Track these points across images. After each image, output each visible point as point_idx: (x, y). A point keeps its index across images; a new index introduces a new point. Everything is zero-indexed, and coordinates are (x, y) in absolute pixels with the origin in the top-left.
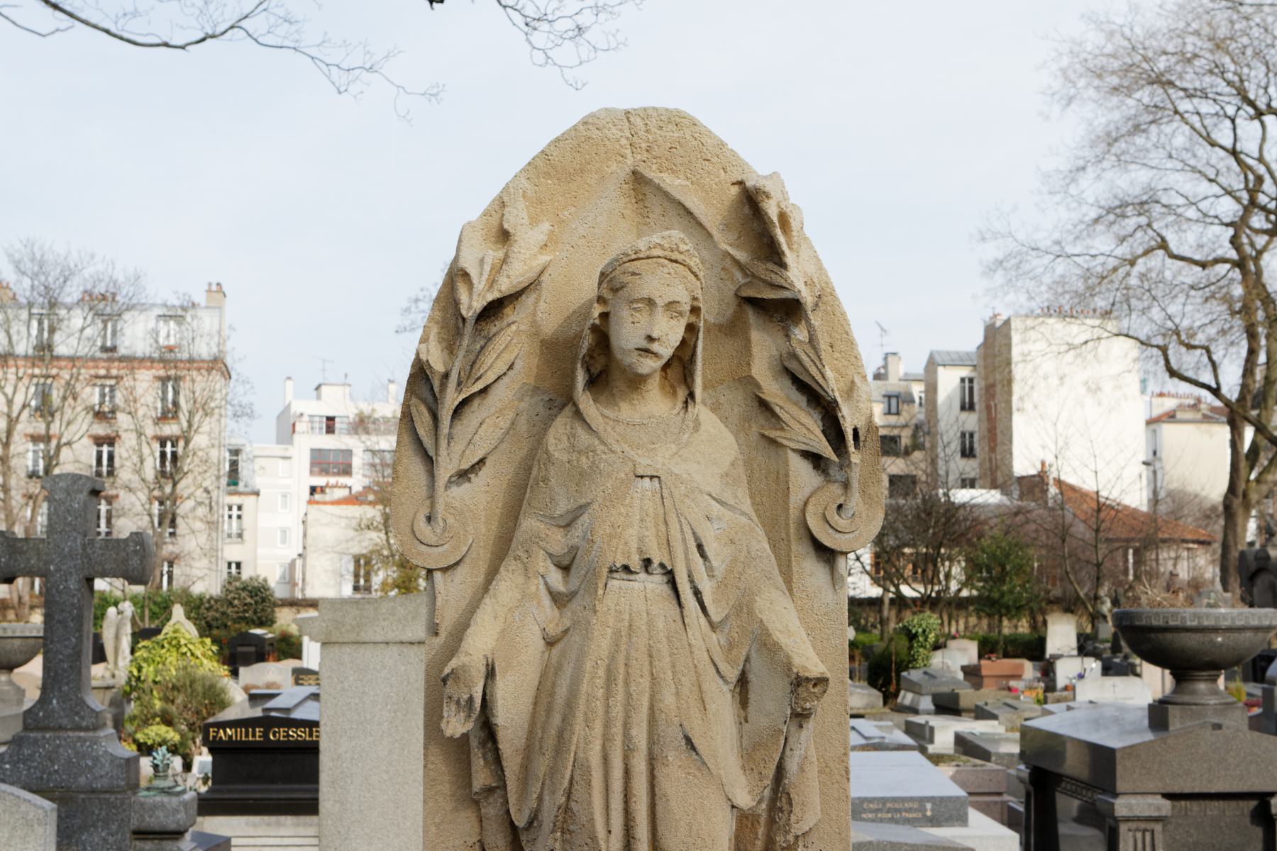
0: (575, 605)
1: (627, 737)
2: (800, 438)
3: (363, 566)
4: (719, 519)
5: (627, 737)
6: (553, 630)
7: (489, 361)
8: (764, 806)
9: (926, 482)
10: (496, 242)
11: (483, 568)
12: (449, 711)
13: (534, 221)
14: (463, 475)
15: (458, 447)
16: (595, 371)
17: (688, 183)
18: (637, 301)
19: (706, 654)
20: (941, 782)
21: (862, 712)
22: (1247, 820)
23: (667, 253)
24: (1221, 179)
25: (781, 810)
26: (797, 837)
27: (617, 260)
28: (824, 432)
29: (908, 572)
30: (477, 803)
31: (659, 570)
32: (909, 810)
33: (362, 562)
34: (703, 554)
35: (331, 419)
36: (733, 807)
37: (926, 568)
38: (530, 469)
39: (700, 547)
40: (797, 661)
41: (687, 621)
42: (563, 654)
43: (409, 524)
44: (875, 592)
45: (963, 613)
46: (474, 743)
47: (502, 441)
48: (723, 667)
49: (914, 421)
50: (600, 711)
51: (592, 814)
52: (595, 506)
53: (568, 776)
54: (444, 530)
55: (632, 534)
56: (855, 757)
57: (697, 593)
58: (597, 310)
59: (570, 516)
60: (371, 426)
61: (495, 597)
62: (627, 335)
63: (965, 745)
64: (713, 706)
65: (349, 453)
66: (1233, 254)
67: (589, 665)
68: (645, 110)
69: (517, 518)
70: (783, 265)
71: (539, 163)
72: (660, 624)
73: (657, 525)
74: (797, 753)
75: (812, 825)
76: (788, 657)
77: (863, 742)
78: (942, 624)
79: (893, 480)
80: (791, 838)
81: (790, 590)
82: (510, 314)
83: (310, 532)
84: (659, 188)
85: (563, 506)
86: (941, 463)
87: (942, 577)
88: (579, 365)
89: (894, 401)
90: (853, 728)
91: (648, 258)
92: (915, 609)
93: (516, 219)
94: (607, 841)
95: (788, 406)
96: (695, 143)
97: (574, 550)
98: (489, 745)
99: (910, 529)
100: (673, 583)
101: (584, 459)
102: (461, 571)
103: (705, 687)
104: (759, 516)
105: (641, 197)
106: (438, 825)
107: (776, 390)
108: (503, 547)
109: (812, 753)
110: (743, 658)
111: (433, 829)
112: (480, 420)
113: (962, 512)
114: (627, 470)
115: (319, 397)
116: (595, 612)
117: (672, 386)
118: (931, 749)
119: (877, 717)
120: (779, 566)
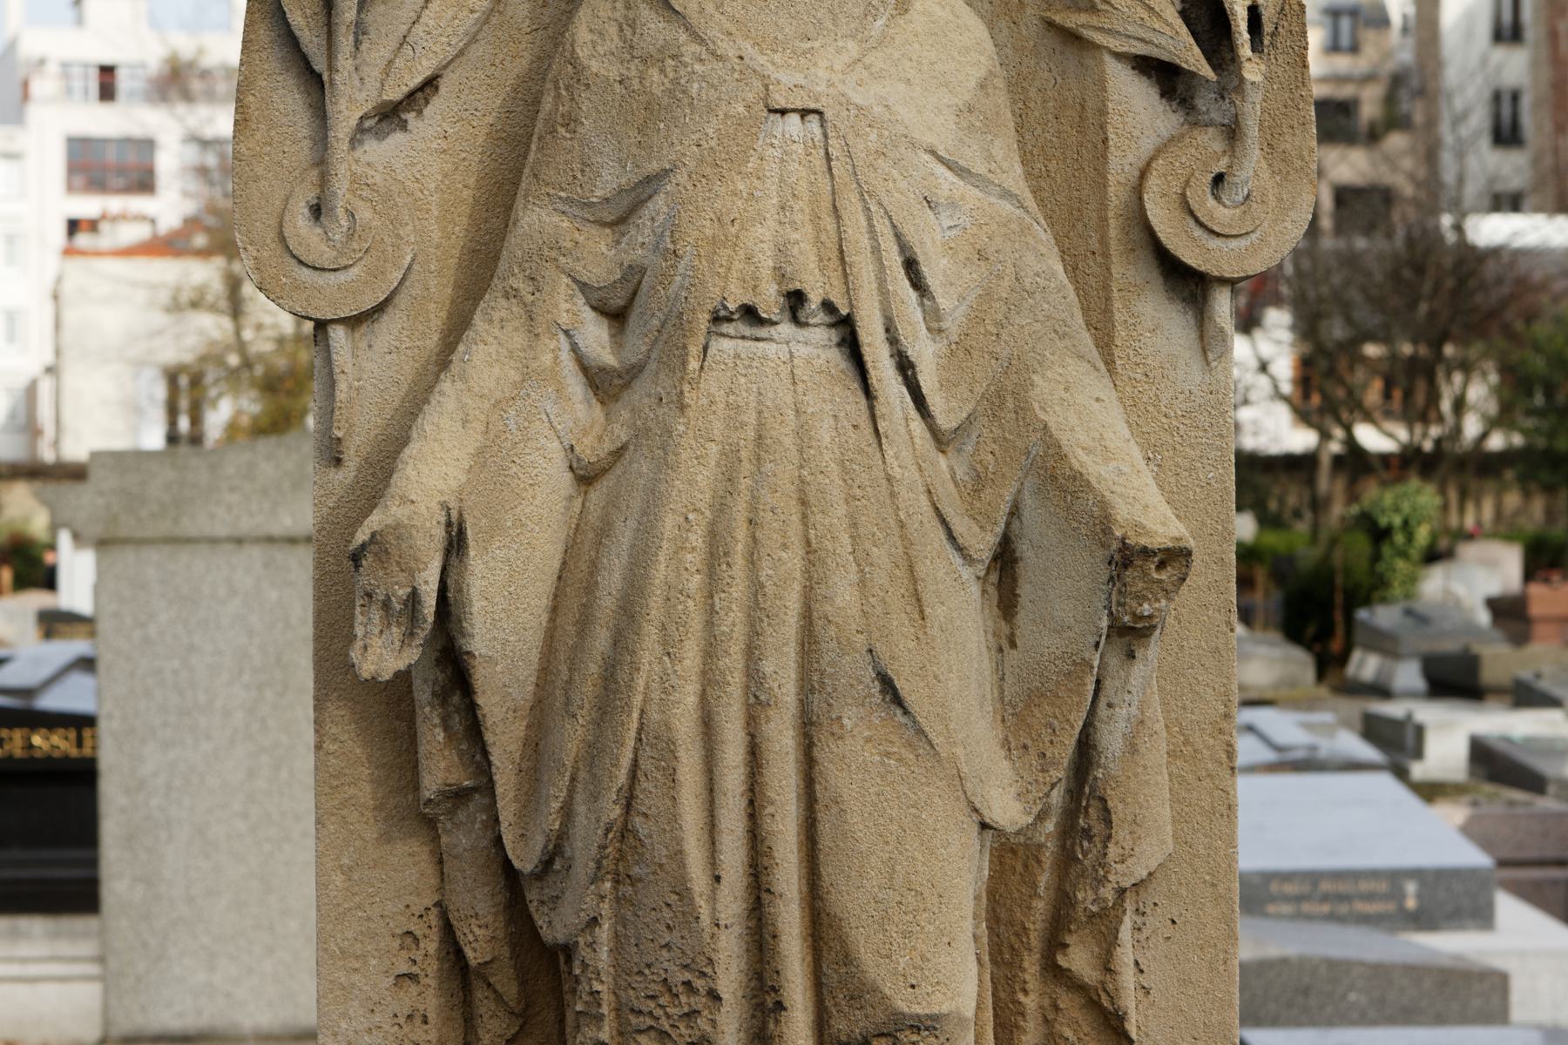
0: (639, 394)
1: (753, 676)
2: (1131, 29)
3: (185, 389)
4: (953, 205)
5: (753, 676)
6: (592, 450)
8: (1050, 826)
9: (1415, 202)
11: (436, 317)
12: (367, 623)
14: (390, 115)
15: (377, 52)
19: (924, 499)
20: (1440, 839)
21: (1269, 695)
25: (1087, 834)
26: (1121, 892)
28: (1183, 14)
29: (1373, 395)
30: (430, 823)
31: (821, 317)
32: (1370, 897)
33: (184, 381)
35: (107, 71)
36: (984, 826)
37: (1412, 389)
38: (537, 101)
39: (911, 265)
40: (1123, 512)
41: (882, 426)
42: (613, 502)
43: (273, 222)
44: (1300, 440)
45: (1490, 484)
46: (423, 693)
47: (474, 39)
48: (961, 525)
49: (1390, 67)
50: (696, 622)
51: (679, 841)
55: (761, 239)
56: (1248, 789)
57: (905, 367)
59: (626, 202)
60: (196, 85)
61: (464, 378)
63: (1488, 761)
64: (941, 610)
65: (147, 145)
67: (669, 524)
69: (509, 208)
73: (816, 218)
74: (1122, 712)
75: (1153, 865)
76: (1104, 505)
77: (1269, 756)
78: (1445, 508)
79: (1343, 196)
80: (1108, 893)
81: (1110, 363)
83: (70, 316)
85: (609, 179)
86: (1447, 159)
87: (1446, 406)
89: (1345, 24)
90: (1250, 729)
92: (1385, 475)
94: (713, 899)
97: (634, 276)
98: (456, 699)
99: (1378, 303)
100: (851, 345)
101: (654, 74)
102: (389, 328)
103: (922, 569)
104: (1041, 203)
106: (347, 871)
108: (480, 270)
109: (1156, 713)
110: (1005, 508)
111: (338, 879)
113: (1490, 269)
114: (750, 96)
115: (80, 21)
116: (682, 408)
118: (1418, 771)
120: (1086, 311)
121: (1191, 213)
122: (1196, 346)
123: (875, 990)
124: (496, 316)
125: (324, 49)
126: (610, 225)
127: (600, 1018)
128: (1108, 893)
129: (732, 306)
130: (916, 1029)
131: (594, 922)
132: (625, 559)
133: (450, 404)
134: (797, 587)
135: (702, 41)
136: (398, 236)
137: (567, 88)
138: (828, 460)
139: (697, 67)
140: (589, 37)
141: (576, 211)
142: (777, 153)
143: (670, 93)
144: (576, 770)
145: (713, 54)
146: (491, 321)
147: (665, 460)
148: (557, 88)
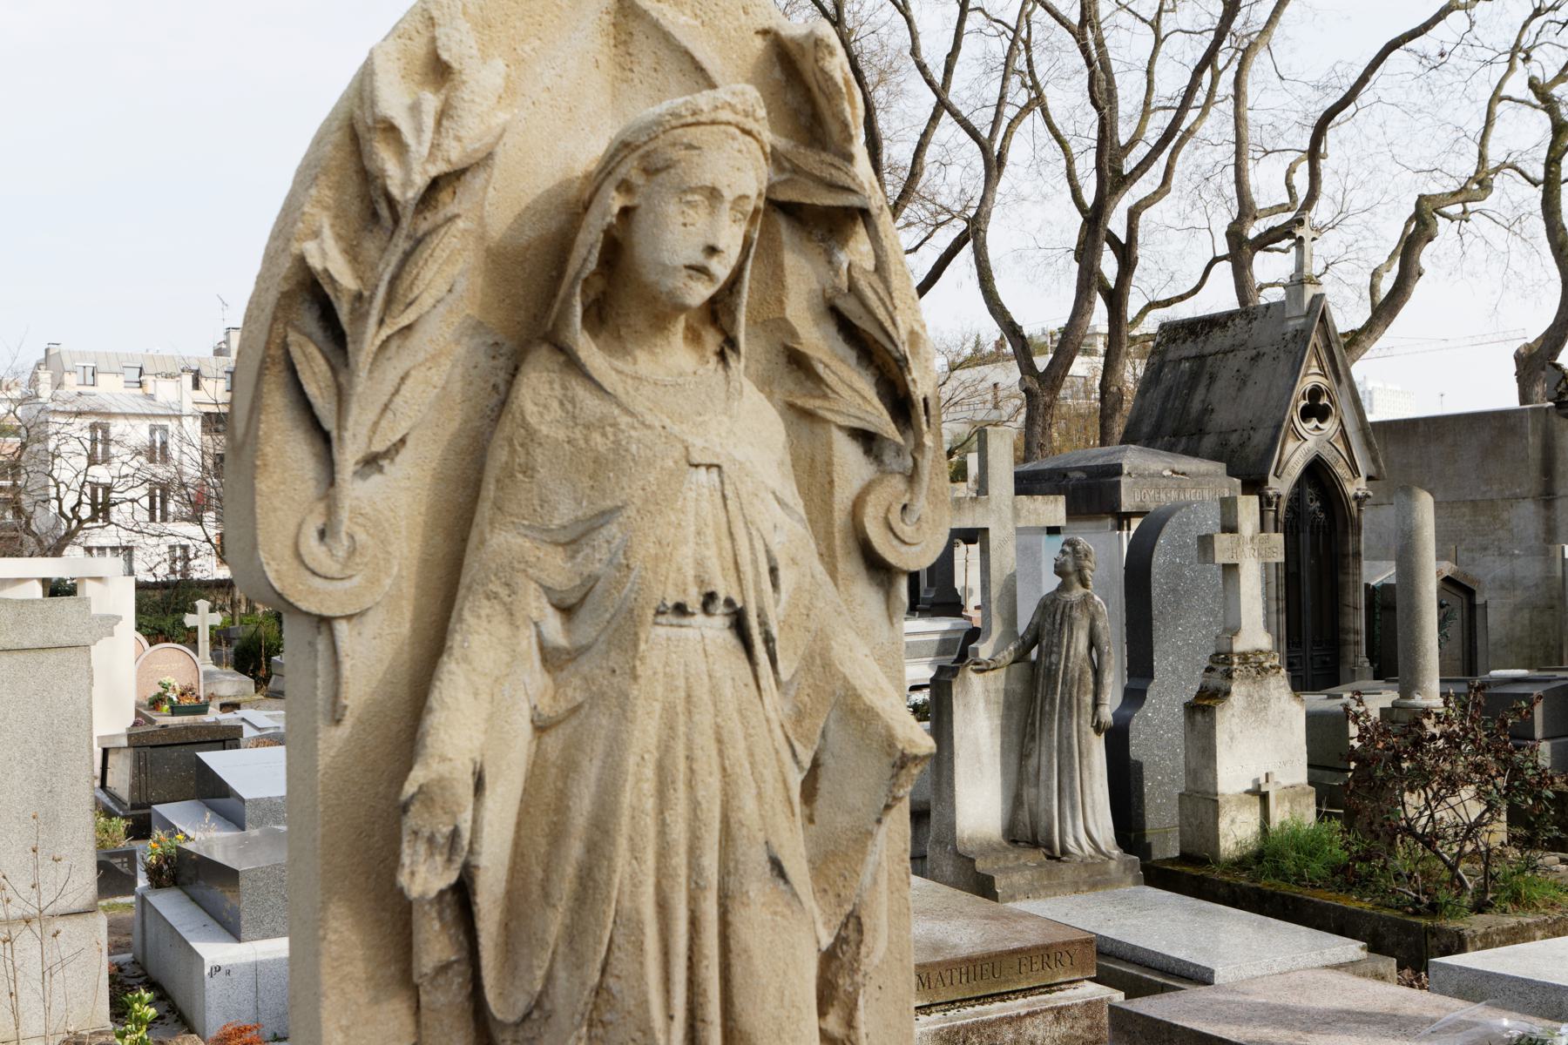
0: (585, 665)
2: (852, 411)
6: (547, 708)
7: (428, 274)
13: (485, 58)
14: (372, 462)
23: (739, 119)
27: (659, 124)
39: (773, 571)
43: (290, 543)
48: (798, 747)
50: (651, 832)
51: (645, 993)
52: (631, 511)
53: (606, 940)
54: (352, 552)
55: (686, 555)
58: (616, 202)
59: (581, 528)
61: (466, 659)
67: (632, 761)
72: (727, 691)
73: (718, 539)
76: (888, 728)
82: (449, 205)
84: (656, 26)
85: (565, 512)
91: (713, 123)
93: (458, 45)
94: (668, 1032)
95: (834, 364)
97: (589, 586)
101: (596, 437)
102: (371, 624)
105: (624, 37)
107: (817, 340)
116: (635, 678)
119: (255, 706)
121: (891, 529)
122: (885, 613)
124: (483, 613)
125: (334, 414)
129: (670, 604)
132: (593, 789)
133: (461, 681)
134: (718, 802)
135: (632, 414)
136: (388, 553)
137: (522, 445)
138: (731, 709)
139: (633, 433)
140: (535, 409)
141: (536, 534)
142: (694, 495)
143: (615, 451)
144: (556, 945)
145: (643, 423)
146: (479, 617)
148: (511, 445)
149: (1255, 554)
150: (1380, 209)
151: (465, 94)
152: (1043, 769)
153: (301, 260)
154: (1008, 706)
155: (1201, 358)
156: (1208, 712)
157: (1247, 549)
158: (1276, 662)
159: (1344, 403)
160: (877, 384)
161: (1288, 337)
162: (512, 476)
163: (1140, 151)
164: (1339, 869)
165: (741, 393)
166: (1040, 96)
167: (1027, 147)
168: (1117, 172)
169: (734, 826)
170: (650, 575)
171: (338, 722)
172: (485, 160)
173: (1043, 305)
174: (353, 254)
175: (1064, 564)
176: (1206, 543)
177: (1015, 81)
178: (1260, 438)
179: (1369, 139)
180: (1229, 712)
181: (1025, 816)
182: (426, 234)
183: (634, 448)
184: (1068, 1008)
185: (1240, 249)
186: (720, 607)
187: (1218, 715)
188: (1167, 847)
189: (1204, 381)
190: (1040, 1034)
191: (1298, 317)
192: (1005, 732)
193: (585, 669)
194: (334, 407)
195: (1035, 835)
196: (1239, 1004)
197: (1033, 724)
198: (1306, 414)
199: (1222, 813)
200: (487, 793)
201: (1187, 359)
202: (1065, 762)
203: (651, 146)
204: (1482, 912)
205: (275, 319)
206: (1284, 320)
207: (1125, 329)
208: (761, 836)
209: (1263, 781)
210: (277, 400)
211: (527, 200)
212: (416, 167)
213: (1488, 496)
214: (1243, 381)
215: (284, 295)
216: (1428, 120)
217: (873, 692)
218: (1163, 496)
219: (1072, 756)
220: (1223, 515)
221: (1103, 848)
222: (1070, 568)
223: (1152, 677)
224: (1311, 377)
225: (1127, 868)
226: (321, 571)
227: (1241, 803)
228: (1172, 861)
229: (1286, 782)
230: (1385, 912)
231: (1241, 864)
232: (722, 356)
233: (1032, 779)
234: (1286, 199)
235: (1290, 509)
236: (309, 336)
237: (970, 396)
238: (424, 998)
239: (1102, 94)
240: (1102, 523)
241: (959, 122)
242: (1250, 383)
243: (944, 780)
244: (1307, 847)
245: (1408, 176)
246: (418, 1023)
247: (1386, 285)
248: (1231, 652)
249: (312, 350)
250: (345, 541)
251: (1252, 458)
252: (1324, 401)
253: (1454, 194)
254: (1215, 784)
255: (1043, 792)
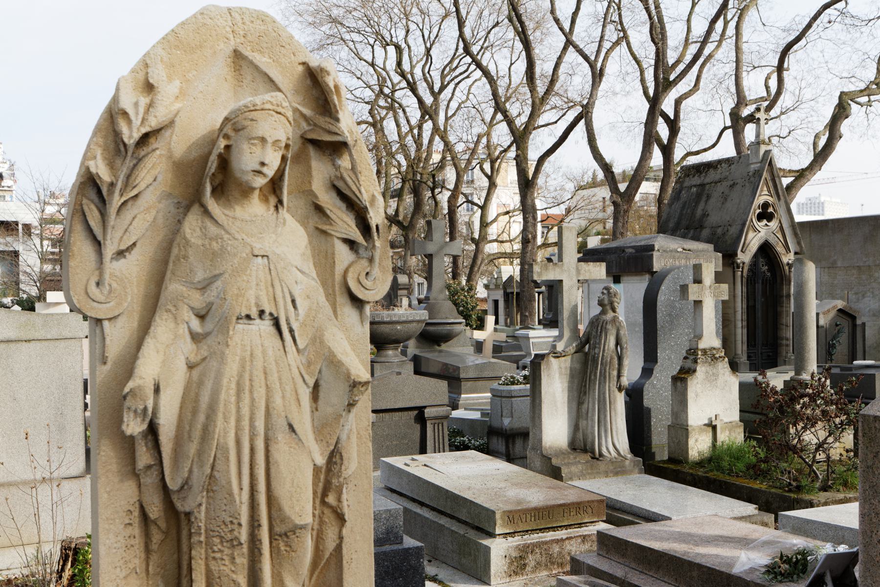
0: (210, 340)
1: (252, 426)
2: (343, 231)
5: (252, 426)
6: (193, 359)
7: (142, 174)
10: (142, 92)
13: (170, 79)
14: (121, 254)
16: (215, 184)
17: (271, 61)
18: (254, 138)
22: (413, 421)
24: (363, 78)
25: (335, 463)
27: (239, 110)
34: (295, 306)
39: (293, 301)
40: (353, 372)
43: (83, 288)
48: (306, 377)
51: (230, 478)
52: (226, 275)
53: (213, 455)
54: (110, 292)
55: (251, 294)
57: (291, 331)
58: (222, 143)
59: (206, 282)
61: (155, 337)
62: (247, 159)
66: (370, 120)
67: (225, 381)
68: (241, 8)
70: (338, 120)
71: (170, 37)
72: (270, 352)
73: (267, 288)
76: (348, 370)
82: (154, 143)
84: (251, 63)
85: (200, 275)
88: (208, 180)
91: (262, 110)
93: (157, 76)
94: (240, 495)
95: (334, 210)
96: (275, 34)
97: (209, 306)
101: (214, 244)
102: (120, 322)
107: (328, 200)
112: (133, 216)
116: (228, 346)
117: (264, 195)
123: (289, 518)
126: (200, 289)
127: (200, 534)
128: (341, 480)
129: (243, 315)
130: (301, 529)
131: (200, 505)
143: (221, 250)
147: (222, 360)
149: (711, 297)
150: (820, 99)
151: (159, 97)
152: (590, 410)
153: (88, 168)
154: (572, 376)
155: (702, 185)
156: (684, 381)
157: (707, 292)
158: (723, 354)
159: (782, 211)
160: (356, 219)
161: (751, 174)
162: (179, 260)
163: (681, 67)
164: (750, 467)
165: (284, 223)
166: (625, 37)
167: (618, 64)
168: (666, 79)
169: (271, 410)
170: (234, 302)
171: (105, 363)
172: (171, 123)
173: (624, 156)
174: (111, 166)
175: (603, 300)
176: (684, 289)
177: (610, 27)
178: (733, 230)
179: (813, 60)
180: (695, 381)
181: (580, 435)
182: (144, 157)
183: (229, 248)
184: (589, 536)
185: (737, 122)
186: (267, 316)
187: (689, 383)
188: (662, 454)
189: (704, 198)
190: (574, 549)
191: (756, 163)
192: (570, 390)
193: (209, 342)
194: (102, 230)
195: (585, 445)
196: (666, 531)
197: (585, 386)
198: (760, 217)
199: (690, 436)
200: (162, 393)
201: (695, 186)
202: (602, 406)
203: (236, 120)
204: (826, 491)
205: (78, 193)
206: (749, 165)
207: (672, 167)
208: (283, 414)
209: (714, 419)
210: (79, 228)
211: (193, 140)
212: (135, 130)
213: (867, 263)
214: (725, 198)
215: (81, 183)
216: (849, 49)
217: (342, 354)
218: (677, 263)
219: (605, 404)
220: (694, 274)
221: (622, 453)
222: (606, 302)
223: (656, 362)
224: (763, 196)
225: (635, 464)
226: (97, 300)
227: (701, 430)
228: (664, 462)
229: (726, 420)
230: (773, 490)
231: (700, 464)
232: (276, 207)
233: (584, 415)
234: (765, 94)
235: (750, 270)
236: (92, 201)
237: (587, 205)
238: (142, 480)
239: (658, 34)
240: (643, 277)
241: (577, 51)
242: (729, 200)
243: (537, 415)
244: (735, 454)
245: (837, 80)
246: (140, 491)
247: (822, 142)
248: (697, 348)
249: (93, 207)
250: (108, 288)
251: (729, 242)
252: (771, 210)
253: (861, 91)
254: (687, 420)
255: (590, 422)
